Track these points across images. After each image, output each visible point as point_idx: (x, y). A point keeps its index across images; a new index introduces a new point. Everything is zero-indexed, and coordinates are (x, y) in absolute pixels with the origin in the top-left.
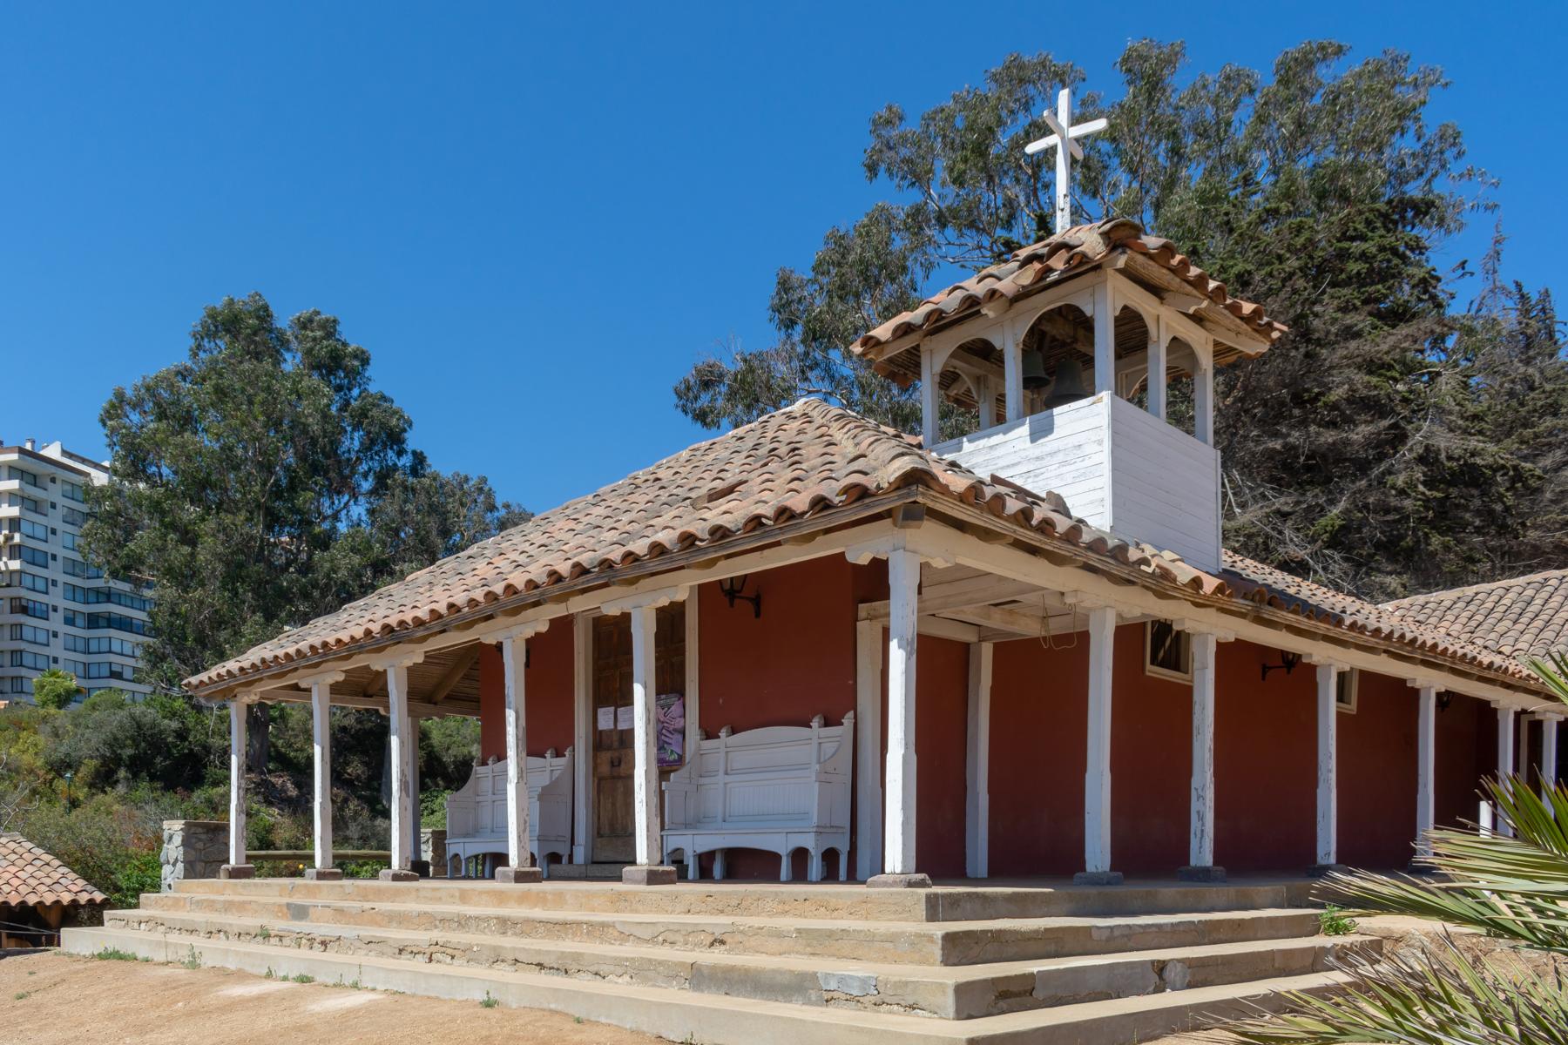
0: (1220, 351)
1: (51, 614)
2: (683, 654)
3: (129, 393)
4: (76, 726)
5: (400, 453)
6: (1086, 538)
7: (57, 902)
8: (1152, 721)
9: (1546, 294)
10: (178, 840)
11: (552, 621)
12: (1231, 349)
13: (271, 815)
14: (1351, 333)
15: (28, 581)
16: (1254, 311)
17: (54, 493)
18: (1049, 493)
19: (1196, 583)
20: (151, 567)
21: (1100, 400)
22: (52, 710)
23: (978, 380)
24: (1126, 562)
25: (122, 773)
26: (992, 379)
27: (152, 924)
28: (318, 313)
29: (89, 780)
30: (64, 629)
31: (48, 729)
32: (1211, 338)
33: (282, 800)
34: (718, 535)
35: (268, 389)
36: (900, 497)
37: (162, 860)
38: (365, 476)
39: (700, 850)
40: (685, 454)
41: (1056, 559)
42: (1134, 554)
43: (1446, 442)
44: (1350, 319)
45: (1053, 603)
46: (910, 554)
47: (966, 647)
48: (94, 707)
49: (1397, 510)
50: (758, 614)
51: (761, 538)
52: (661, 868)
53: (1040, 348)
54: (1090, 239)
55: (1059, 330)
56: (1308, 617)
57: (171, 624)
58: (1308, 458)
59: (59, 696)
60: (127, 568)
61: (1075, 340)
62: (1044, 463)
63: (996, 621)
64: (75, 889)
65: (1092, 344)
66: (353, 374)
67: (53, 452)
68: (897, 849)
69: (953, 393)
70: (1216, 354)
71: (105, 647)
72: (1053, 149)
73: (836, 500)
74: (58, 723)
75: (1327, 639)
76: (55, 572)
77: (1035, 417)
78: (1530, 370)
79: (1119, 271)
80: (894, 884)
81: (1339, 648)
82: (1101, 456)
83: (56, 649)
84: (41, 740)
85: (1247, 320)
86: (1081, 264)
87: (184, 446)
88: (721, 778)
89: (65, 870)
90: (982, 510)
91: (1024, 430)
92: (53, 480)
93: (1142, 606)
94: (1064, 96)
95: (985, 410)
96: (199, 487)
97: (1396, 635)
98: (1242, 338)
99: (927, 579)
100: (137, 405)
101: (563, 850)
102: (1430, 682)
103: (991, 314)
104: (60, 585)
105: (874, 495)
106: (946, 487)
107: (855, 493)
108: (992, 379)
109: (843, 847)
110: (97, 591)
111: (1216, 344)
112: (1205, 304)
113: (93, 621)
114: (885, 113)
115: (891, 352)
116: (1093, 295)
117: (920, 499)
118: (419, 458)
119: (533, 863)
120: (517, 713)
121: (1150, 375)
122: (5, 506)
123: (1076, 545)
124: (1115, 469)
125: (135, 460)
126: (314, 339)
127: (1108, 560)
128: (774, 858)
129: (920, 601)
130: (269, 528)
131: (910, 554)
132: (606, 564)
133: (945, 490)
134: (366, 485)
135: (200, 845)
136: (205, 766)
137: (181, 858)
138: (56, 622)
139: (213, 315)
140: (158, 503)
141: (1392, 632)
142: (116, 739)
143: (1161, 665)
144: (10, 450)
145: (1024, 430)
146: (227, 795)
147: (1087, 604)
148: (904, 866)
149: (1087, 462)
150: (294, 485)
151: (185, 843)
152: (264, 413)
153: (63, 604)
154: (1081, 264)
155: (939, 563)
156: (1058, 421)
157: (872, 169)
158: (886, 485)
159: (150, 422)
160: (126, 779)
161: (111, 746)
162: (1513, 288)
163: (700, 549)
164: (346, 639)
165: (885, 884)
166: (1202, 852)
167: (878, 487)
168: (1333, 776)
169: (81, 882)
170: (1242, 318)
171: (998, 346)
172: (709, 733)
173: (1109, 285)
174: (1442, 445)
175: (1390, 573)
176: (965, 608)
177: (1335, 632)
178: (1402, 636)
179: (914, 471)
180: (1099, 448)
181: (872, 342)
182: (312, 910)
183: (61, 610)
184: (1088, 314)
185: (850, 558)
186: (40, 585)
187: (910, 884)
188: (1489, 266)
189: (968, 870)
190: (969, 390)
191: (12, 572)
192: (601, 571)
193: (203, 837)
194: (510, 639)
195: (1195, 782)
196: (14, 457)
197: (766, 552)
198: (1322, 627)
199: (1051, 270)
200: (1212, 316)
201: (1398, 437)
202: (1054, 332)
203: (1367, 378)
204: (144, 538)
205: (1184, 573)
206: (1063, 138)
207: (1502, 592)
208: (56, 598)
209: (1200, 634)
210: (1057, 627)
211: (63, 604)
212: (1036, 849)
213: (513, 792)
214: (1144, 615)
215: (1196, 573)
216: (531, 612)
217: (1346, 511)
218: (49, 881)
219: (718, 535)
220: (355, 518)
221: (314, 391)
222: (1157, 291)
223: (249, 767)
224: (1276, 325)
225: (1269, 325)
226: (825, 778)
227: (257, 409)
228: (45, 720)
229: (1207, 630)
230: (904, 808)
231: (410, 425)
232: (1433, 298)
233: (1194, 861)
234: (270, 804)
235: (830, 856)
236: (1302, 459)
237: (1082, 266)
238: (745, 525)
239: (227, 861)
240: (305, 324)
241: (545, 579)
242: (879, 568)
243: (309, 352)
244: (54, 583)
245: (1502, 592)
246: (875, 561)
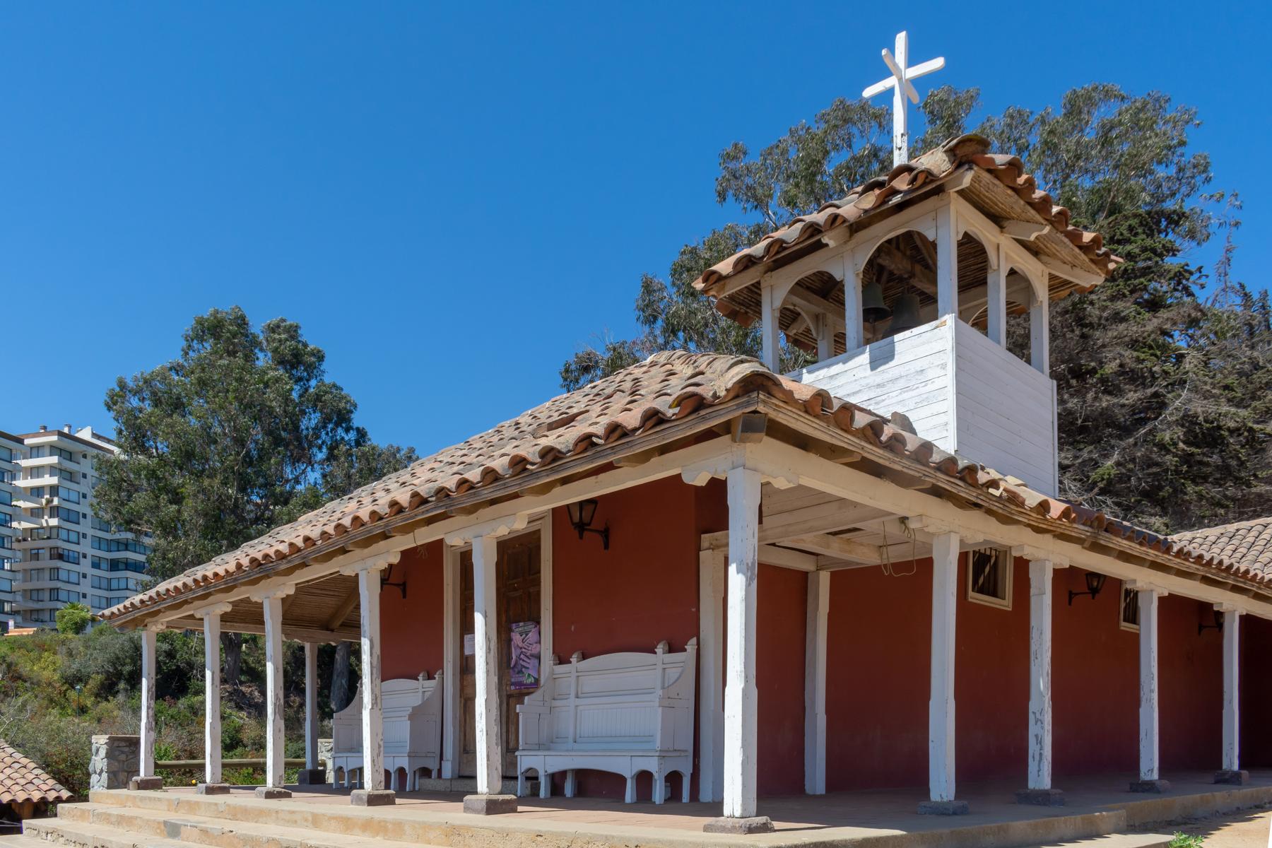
0: (1056, 285)
1: (82, 560)
2: (539, 584)
3: (131, 384)
4: (87, 647)
5: (347, 430)
6: (936, 458)
7: (28, 800)
8: (992, 649)
9: (1265, 295)
10: (103, 753)
11: (404, 553)
12: (1066, 283)
13: (240, 718)
14: (1118, 318)
15: (63, 534)
16: (1092, 240)
17: (86, 466)
18: (895, 414)
19: (1044, 507)
20: (148, 521)
21: (944, 323)
22: (70, 635)
23: (817, 318)
24: (974, 484)
25: (122, 685)
26: (830, 317)
27: (55, 835)
28: (284, 321)
29: (95, 691)
30: (91, 571)
31: (65, 651)
32: (1047, 271)
33: (250, 706)
34: (550, 457)
35: (240, 380)
36: (739, 406)
37: (91, 769)
38: (320, 448)
39: (550, 771)
40: (547, 404)
41: (901, 480)
42: (982, 477)
43: (1199, 407)
44: (1119, 305)
45: (894, 530)
46: (750, 473)
47: (805, 575)
48: (101, 633)
49: (1157, 464)
50: (606, 547)
51: (592, 459)
52: (501, 797)
53: (878, 281)
54: (935, 161)
55: (897, 264)
56: (1141, 544)
57: (164, 566)
58: (1084, 421)
59: (76, 623)
60: (129, 522)
61: (912, 275)
62: (885, 390)
63: (834, 550)
64: (45, 787)
65: (934, 282)
66: (310, 368)
67: (85, 434)
68: (735, 786)
69: (792, 332)
70: (1052, 288)
71: (123, 585)
72: (890, 92)
73: (670, 413)
74: (72, 645)
75: (1155, 566)
76: (85, 527)
77: (875, 345)
78: (1255, 354)
79: (961, 193)
80: (733, 830)
81: (1160, 573)
82: (945, 380)
83: (85, 587)
84: (60, 659)
85: (1085, 249)
86: (924, 184)
87: (172, 426)
88: (572, 701)
89: (39, 771)
90: (828, 423)
91: (865, 358)
92: (85, 456)
93: (982, 531)
94: (901, 40)
95: (823, 346)
96: (187, 457)
97: (1215, 562)
98: (1078, 271)
99: (770, 504)
100: (137, 392)
101: (433, 765)
102: (1234, 605)
103: (832, 243)
104: (89, 537)
105: (711, 406)
106: (791, 393)
107: (690, 404)
108: (830, 317)
109: (686, 770)
110: (118, 542)
111: (1052, 277)
112: (1047, 229)
113: (114, 565)
114: (729, 149)
115: (733, 288)
116: (935, 219)
117: (761, 408)
118: (362, 434)
119: (387, 787)
120: (371, 641)
121: (990, 306)
122: (47, 476)
123: (926, 464)
124: (959, 393)
125: (137, 437)
126: (280, 341)
127: (956, 482)
128: (620, 780)
129: (760, 530)
130: (242, 489)
131: (750, 473)
132: (442, 492)
133: (789, 397)
134: (320, 456)
135: (123, 757)
136: (189, 679)
137: (105, 769)
138: (85, 567)
139: (200, 322)
140: (154, 471)
141: (1212, 559)
142: (118, 658)
143: (981, 591)
144: (51, 433)
145: (865, 358)
146: (203, 702)
147: (931, 529)
148: (744, 809)
149: (930, 387)
150: (263, 456)
151: (108, 755)
152: (236, 398)
153: (90, 552)
154: (924, 184)
155: (781, 483)
156: (898, 347)
157: (722, 196)
158: (723, 393)
159: (147, 409)
160: (126, 690)
161: (114, 664)
162: (1237, 287)
163: (532, 473)
164: (222, 573)
165: (723, 829)
166: (1040, 775)
167: (715, 396)
168: (1155, 696)
169: (51, 782)
170: (1080, 248)
171: (838, 277)
172: (562, 659)
173: (952, 208)
174: (1199, 410)
175: (1152, 515)
176: (804, 537)
177: (1162, 558)
178: (1221, 562)
179: (755, 375)
180: (943, 372)
181: (714, 277)
182: (183, 829)
183: (89, 557)
184: (931, 238)
185: (687, 479)
186: (73, 537)
187: (751, 830)
188: (1222, 270)
189: (807, 787)
190: (808, 330)
191: (51, 528)
192: (439, 500)
193: (126, 749)
194: (367, 569)
195: (1033, 706)
196: (55, 438)
197: (602, 476)
198: (1152, 554)
199: (895, 192)
200: (1053, 247)
201: (1157, 405)
202: (893, 267)
203: (1135, 354)
204: (141, 499)
205: (1032, 498)
206: (900, 79)
207: (1261, 528)
208: (86, 547)
209: (1037, 560)
210: (896, 555)
211: (90, 552)
212: (873, 770)
213: (377, 718)
214: (986, 542)
215: (1043, 497)
216: (382, 544)
217: (1118, 464)
218: (23, 782)
219: (550, 457)
220: (312, 481)
221: (277, 380)
222: (997, 219)
223: (224, 678)
224: (1113, 257)
225: (1106, 255)
226: (668, 704)
227: (231, 396)
228: (63, 643)
229: (1049, 556)
230: (744, 746)
231: (355, 406)
232: (1186, 289)
233: (1032, 785)
234: (241, 709)
235: (673, 779)
236: (1080, 421)
237: (929, 188)
238: (576, 444)
239: (137, 772)
240: (273, 329)
241: (388, 510)
242: (718, 488)
243: (275, 351)
244: (84, 536)
245: (1261, 528)
246: (713, 481)
